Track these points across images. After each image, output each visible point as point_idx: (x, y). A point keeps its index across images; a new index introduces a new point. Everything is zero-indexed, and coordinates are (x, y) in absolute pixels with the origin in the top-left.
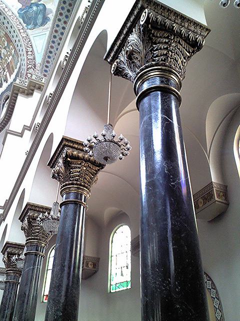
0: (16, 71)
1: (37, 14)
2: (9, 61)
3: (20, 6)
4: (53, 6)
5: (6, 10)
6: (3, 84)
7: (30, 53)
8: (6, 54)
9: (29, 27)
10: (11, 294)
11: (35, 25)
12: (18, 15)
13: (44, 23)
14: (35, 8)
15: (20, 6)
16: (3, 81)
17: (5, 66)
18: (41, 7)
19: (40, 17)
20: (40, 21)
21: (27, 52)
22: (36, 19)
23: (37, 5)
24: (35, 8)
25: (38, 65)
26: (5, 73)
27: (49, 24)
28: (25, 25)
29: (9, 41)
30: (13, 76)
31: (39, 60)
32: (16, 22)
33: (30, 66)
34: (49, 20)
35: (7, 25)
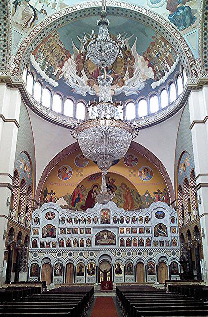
0: (175, 64)
1: (184, 16)
2: (167, 56)
3: (169, 13)
4: (196, 6)
5: (160, 20)
6: (165, 74)
7: (188, 52)
8: (163, 50)
9: (181, 28)
10: (134, 220)
11: (185, 25)
12: (169, 21)
13: (192, 22)
14: (181, 11)
15: (169, 13)
16: (165, 71)
17: (164, 59)
18: (186, 9)
19: (187, 17)
20: (188, 21)
21: (186, 51)
22: (184, 20)
23: (183, 9)
24: (181, 11)
25: (197, 60)
26: (165, 65)
27: (198, 23)
28: (177, 28)
29: (166, 42)
30: (174, 67)
31: (196, 57)
32: (170, 27)
33: (191, 63)
34: (196, 19)
35: (172, 41)
